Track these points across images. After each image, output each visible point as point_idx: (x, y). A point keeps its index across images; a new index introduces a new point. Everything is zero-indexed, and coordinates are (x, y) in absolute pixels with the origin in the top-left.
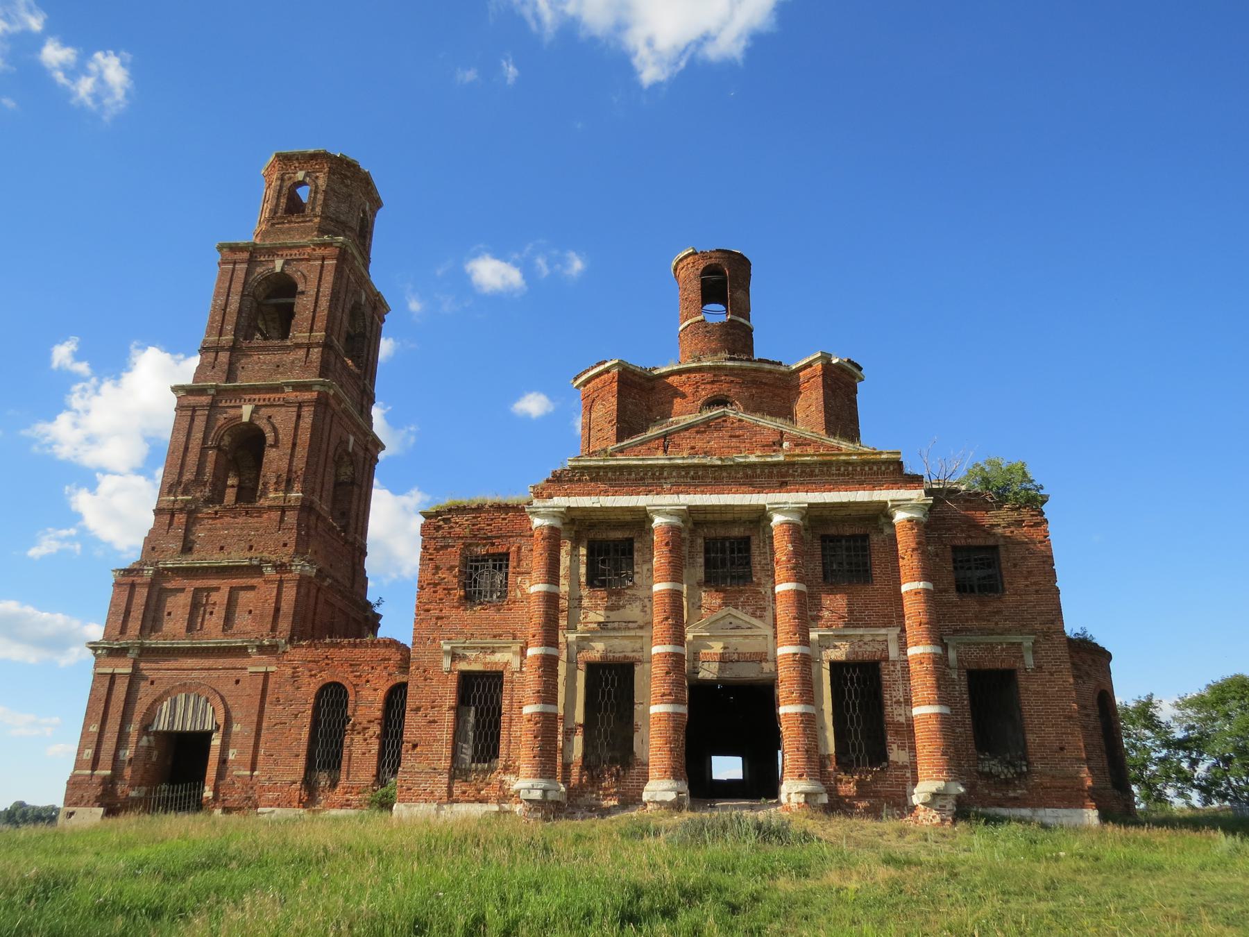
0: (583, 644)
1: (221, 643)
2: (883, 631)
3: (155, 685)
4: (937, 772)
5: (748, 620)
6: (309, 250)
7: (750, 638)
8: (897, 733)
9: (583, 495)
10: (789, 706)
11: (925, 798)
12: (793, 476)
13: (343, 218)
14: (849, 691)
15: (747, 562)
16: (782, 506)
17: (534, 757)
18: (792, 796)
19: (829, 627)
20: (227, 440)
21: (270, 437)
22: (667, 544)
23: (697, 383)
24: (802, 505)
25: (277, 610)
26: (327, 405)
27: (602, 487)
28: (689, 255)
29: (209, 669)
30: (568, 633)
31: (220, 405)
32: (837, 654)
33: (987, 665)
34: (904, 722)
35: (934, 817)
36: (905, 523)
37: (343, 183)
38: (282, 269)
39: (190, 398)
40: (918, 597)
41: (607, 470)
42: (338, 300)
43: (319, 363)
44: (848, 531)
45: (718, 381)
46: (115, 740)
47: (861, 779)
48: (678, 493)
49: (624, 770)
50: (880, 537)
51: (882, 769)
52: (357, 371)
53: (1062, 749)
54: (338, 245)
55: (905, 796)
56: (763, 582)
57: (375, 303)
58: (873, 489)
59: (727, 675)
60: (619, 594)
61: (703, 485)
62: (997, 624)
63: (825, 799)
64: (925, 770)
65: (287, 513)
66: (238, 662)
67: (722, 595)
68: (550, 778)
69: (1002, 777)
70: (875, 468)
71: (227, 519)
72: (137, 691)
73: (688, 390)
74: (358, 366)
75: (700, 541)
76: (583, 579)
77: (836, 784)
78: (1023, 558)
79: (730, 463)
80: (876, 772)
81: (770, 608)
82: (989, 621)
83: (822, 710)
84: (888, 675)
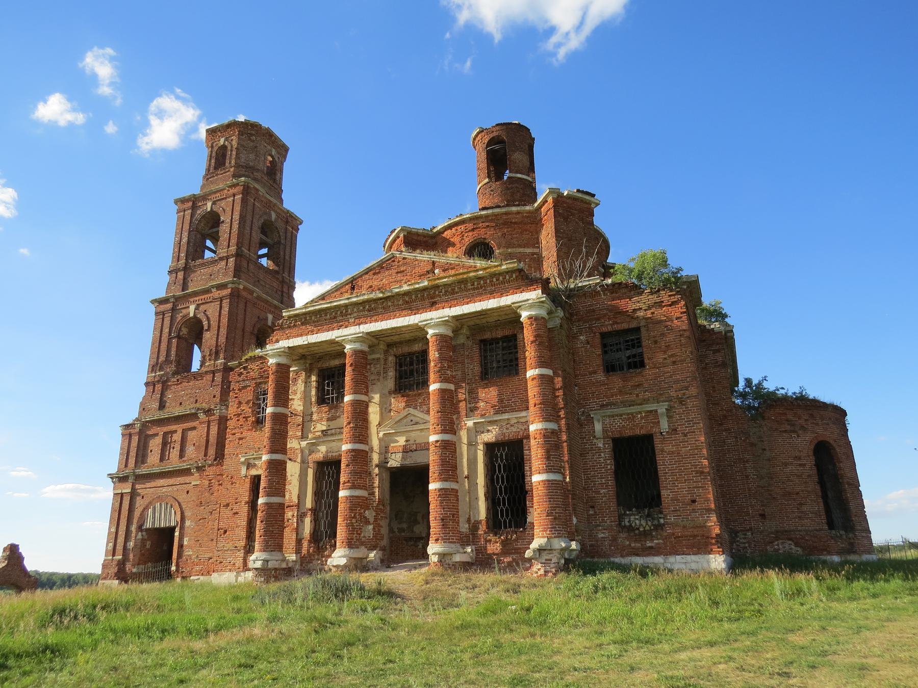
0: (312, 448)
1: (176, 467)
3: (144, 499)
6: (226, 191)
9: (298, 336)
13: (251, 164)
16: (429, 322)
17: (260, 536)
19: (482, 416)
20: (185, 331)
21: (205, 323)
23: (462, 232)
24: (443, 319)
25: (207, 441)
26: (239, 296)
27: (310, 328)
28: (478, 133)
29: (172, 485)
30: (302, 441)
31: (178, 308)
32: (488, 437)
33: (628, 433)
35: (539, 569)
37: (250, 139)
38: (211, 208)
39: (161, 306)
41: (311, 315)
42: (245, 222)
44: (500, 334)
45: (476, 228)
46: (124, 536)
48: (359, 324)
53: (694, 501)
58: (501, 295)
59: (408, 462)
61: (376, 315)
62: (637, 396)
65: (216, 374)
66: (187, 479)
68: (272, 551)
69: (641, 529)
71: (185, 384)
72: (135, 503)
73: (456, 240)
75: (391, 359)
76: (313, 399)
77: (486, 544)
78: (663, 335)
79: (389, 294)
82: (631, 394)
83: (477, 484)
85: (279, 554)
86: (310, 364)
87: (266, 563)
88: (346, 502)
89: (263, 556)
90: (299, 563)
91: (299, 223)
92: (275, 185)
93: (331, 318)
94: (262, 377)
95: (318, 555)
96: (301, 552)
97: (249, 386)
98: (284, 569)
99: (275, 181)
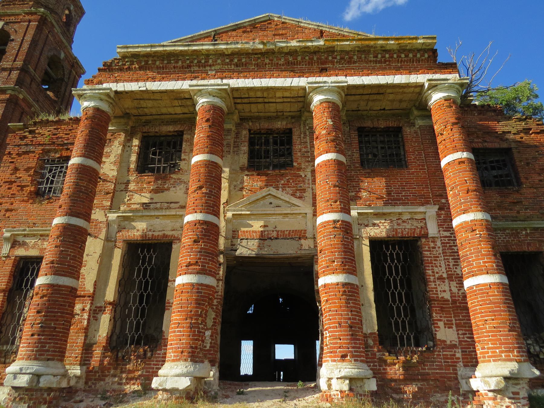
2: (422, 209)
4: (506, 351)
5: (288, 200)
6: (21, 17)
7: (290, 216)
8: (442, 309)
9: (132, 81)
10: (330, 276)
11: (498, 383)
12: (332, 62)
14: (390, 267)
15: (290, 153)
16: (322, 85)
17: (32, 335)
18: (334, 382)
22: (208, 120)
27: (150, 74)
30: (110, 212)
32: (376, 231)
33: (515, 249)
34: (449, 298)
36: (443, 102)
40: (463, 166)
41: (155, 58)
43: (15, 79)
44: (382, 124)
47: (407, 360)
49: (152, 351)
50: (412, 130)
51: (428, 349)
52: (56, 99)
54: (40, 14)
55: (456, 379)
56: (303, 167)
57: (73, 64)
58: (410, 73)
59: (265, 252)
60: (165, 179)
61: (246, 72)
62: (518, 212)
63: (372, 385)
64: (488, 348)
67: (264, 178)
68: (48, 360)
70: (411, 55)
74: (57, 97)
75: (245, 133)
76: (132, 166)
78: (535, 158)
80: (421, 352)
81: (310, 190)
82: (511, 210)
84: (430, 251)
85: (59, 364)
86: (132, 127)
87: (36, 379)
88: (191, 292)
89: (34, 366)
90: (83, 380)
91: (82, 72)
92: (68, 33)
93: (182, 66)
94: (53, 143)
95: (115, 369)
96: (90, 364)
97: (34, 152)
98: (61, 390)
99: (68, 30)
